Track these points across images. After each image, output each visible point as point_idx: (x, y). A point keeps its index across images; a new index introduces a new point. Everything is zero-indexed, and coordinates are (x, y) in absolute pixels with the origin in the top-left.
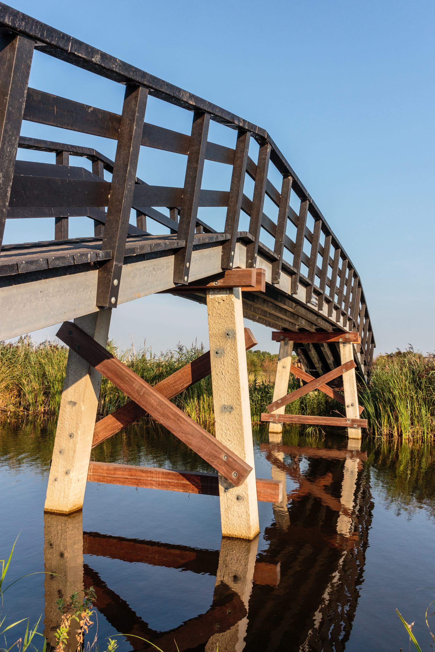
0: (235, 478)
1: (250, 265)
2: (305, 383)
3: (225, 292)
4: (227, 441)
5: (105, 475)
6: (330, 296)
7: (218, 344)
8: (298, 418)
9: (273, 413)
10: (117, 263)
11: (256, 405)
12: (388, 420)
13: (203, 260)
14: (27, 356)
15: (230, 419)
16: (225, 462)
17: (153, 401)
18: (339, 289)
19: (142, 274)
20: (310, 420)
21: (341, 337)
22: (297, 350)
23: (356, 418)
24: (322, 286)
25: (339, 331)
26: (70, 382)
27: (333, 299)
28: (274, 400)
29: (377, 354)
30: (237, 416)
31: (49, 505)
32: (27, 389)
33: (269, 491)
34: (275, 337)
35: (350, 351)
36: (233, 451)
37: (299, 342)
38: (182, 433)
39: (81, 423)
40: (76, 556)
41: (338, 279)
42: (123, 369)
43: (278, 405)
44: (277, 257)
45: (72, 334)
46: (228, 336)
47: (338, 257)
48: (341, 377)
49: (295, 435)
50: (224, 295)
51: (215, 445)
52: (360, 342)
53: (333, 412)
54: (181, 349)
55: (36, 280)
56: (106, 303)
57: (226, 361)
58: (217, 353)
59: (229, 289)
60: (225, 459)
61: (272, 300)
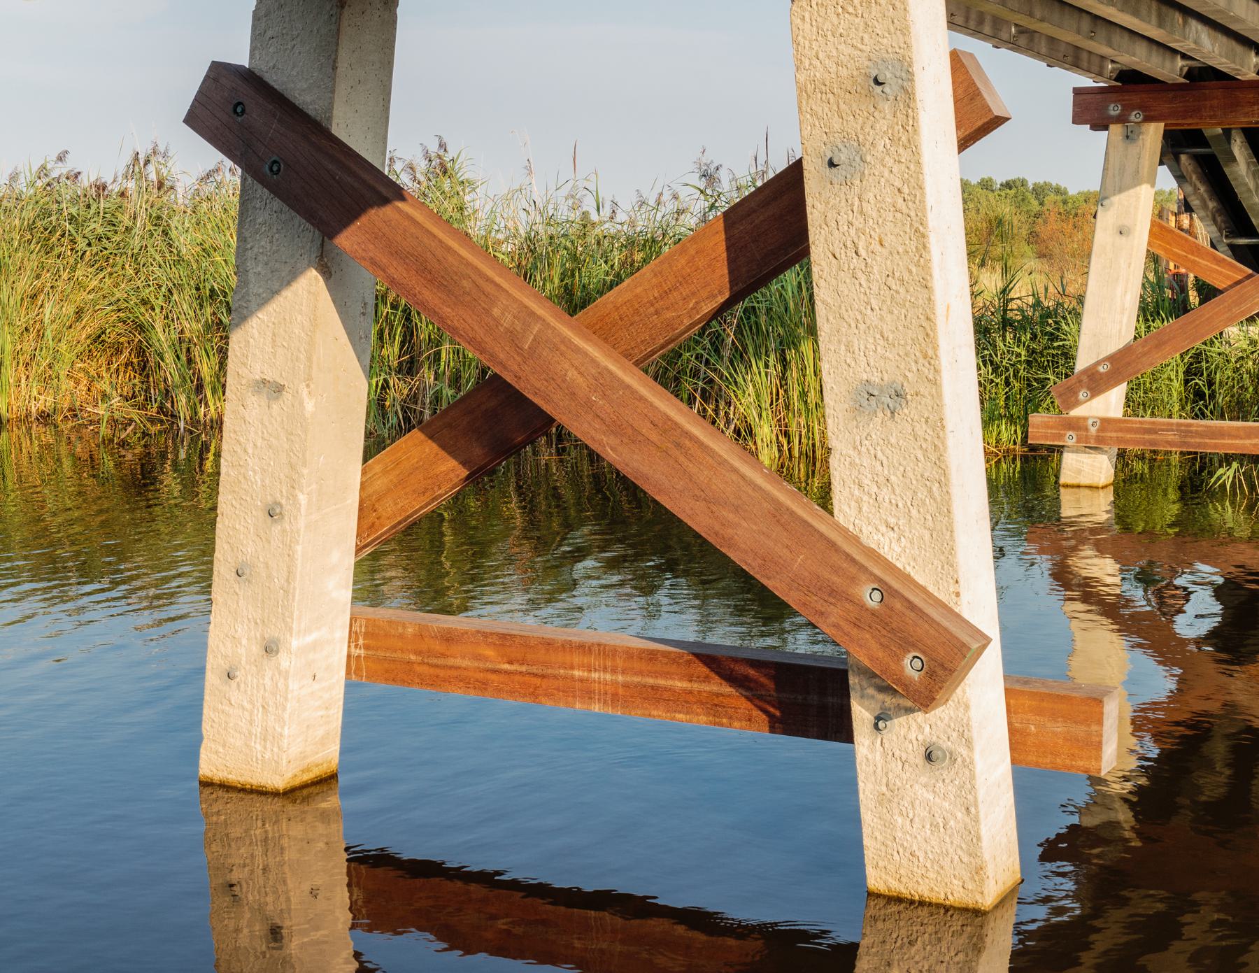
0: (916, 676)
2: (1208, 293)
4: (883, 529)
5: (413, 657)
8: (1177, 430)
11: (1007, 383)
15: (893, 441)
16: (873, 613)
17: (572, 374)
20: (1231, 436)
22: (1177, 160)
26: (253, 305)
28: (1083, 361)
30: (921, 429)
34: (1089, 110)
36: (909, 570)
37: (1189, 123)
39: (304, 464)
42: (449, 249)
43: (1096, 383)
45: (243, 111)
46: (878, 89)
51: (832, 545)
54: (709, 177)
57: (871, 196)
58: (832, 164)
60: (872, 600)
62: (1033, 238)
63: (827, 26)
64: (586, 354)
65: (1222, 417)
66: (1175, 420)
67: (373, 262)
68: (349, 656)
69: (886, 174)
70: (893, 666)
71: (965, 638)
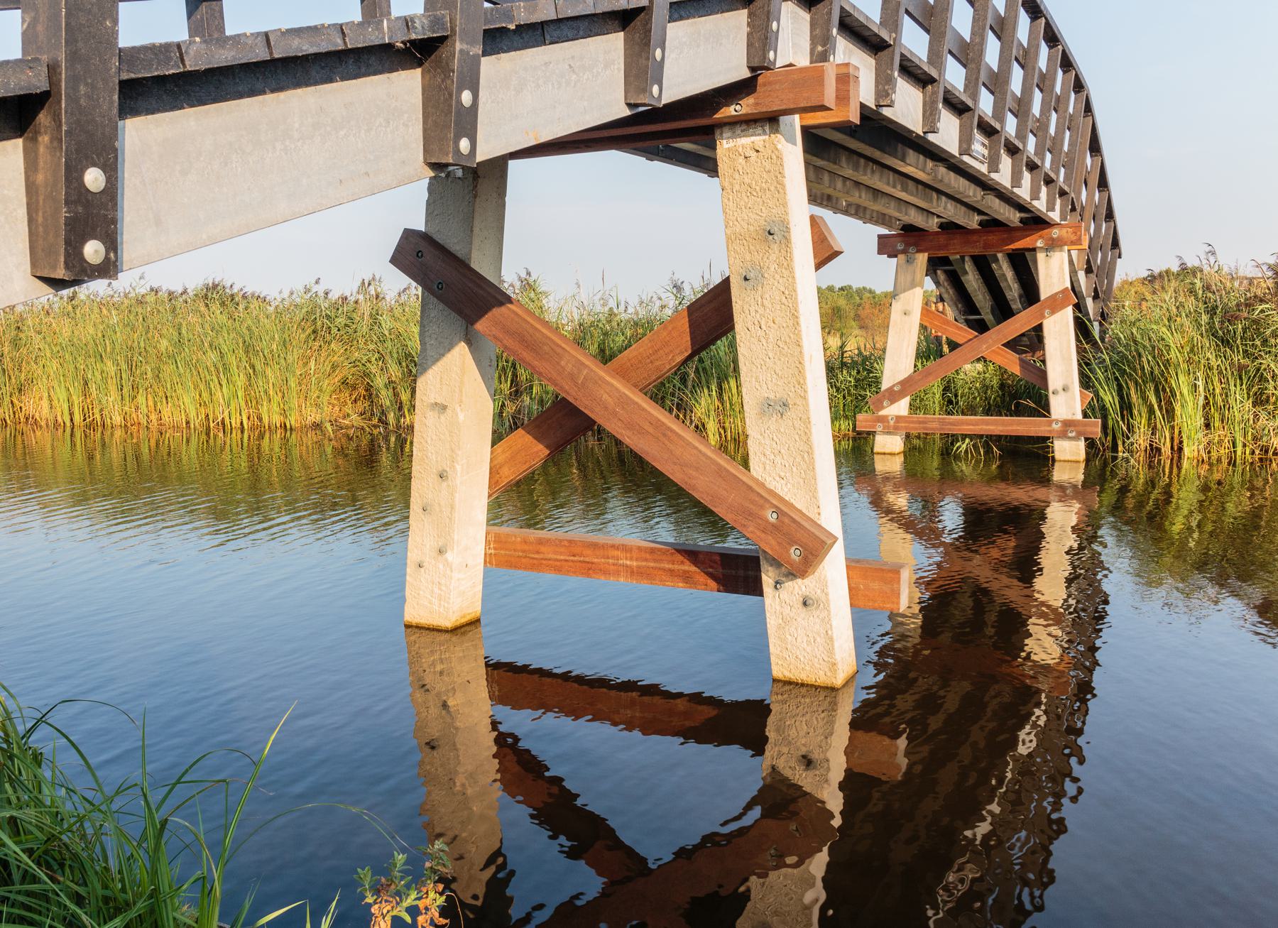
1: (821, 54)
2: (953, 346)
3: (759, 130)
6: (1017, 136)
7: (748, 258)
8: (938, 422)
9: (882, 413)
10: (465, 47)
12: (1150, 419)
13: (698, 46)
14: (375, 317)
16: (773, 525)
17: (605, 396)
18: (1038, 120)
19: (541, 82)
21: (1041, 237)
22: (936, 273)
23: (1075, 418)
24: (999, 113)
25: (1036, 222)
27: (1025, 144)
28: (885, 385)
29: (1129, 269)
31: (413, 613)
32: (379, 382)
33: (876, 585)
34: (885, 247)
35: (1062, 269)
37: (941, 254)
38: (675, 464)
40: (475, 709)
41: (1038, 96)
42: (537, 329)
43: (893, 396)
44: (887, 38)
47: (1037, 38)
48: (1039, 329)
49: (931, 460)
50: (758, 138)
51: (750, 488)
52: (1085, 245)
53: (1018, 405)
54: (678, 287)
55: (249, 96)
56: (447, 155)
58: (746, 279)
59: (770, 120)
60: (772, 518)
61: (877, 154)
62: (857, 317)
71: (824, 538)
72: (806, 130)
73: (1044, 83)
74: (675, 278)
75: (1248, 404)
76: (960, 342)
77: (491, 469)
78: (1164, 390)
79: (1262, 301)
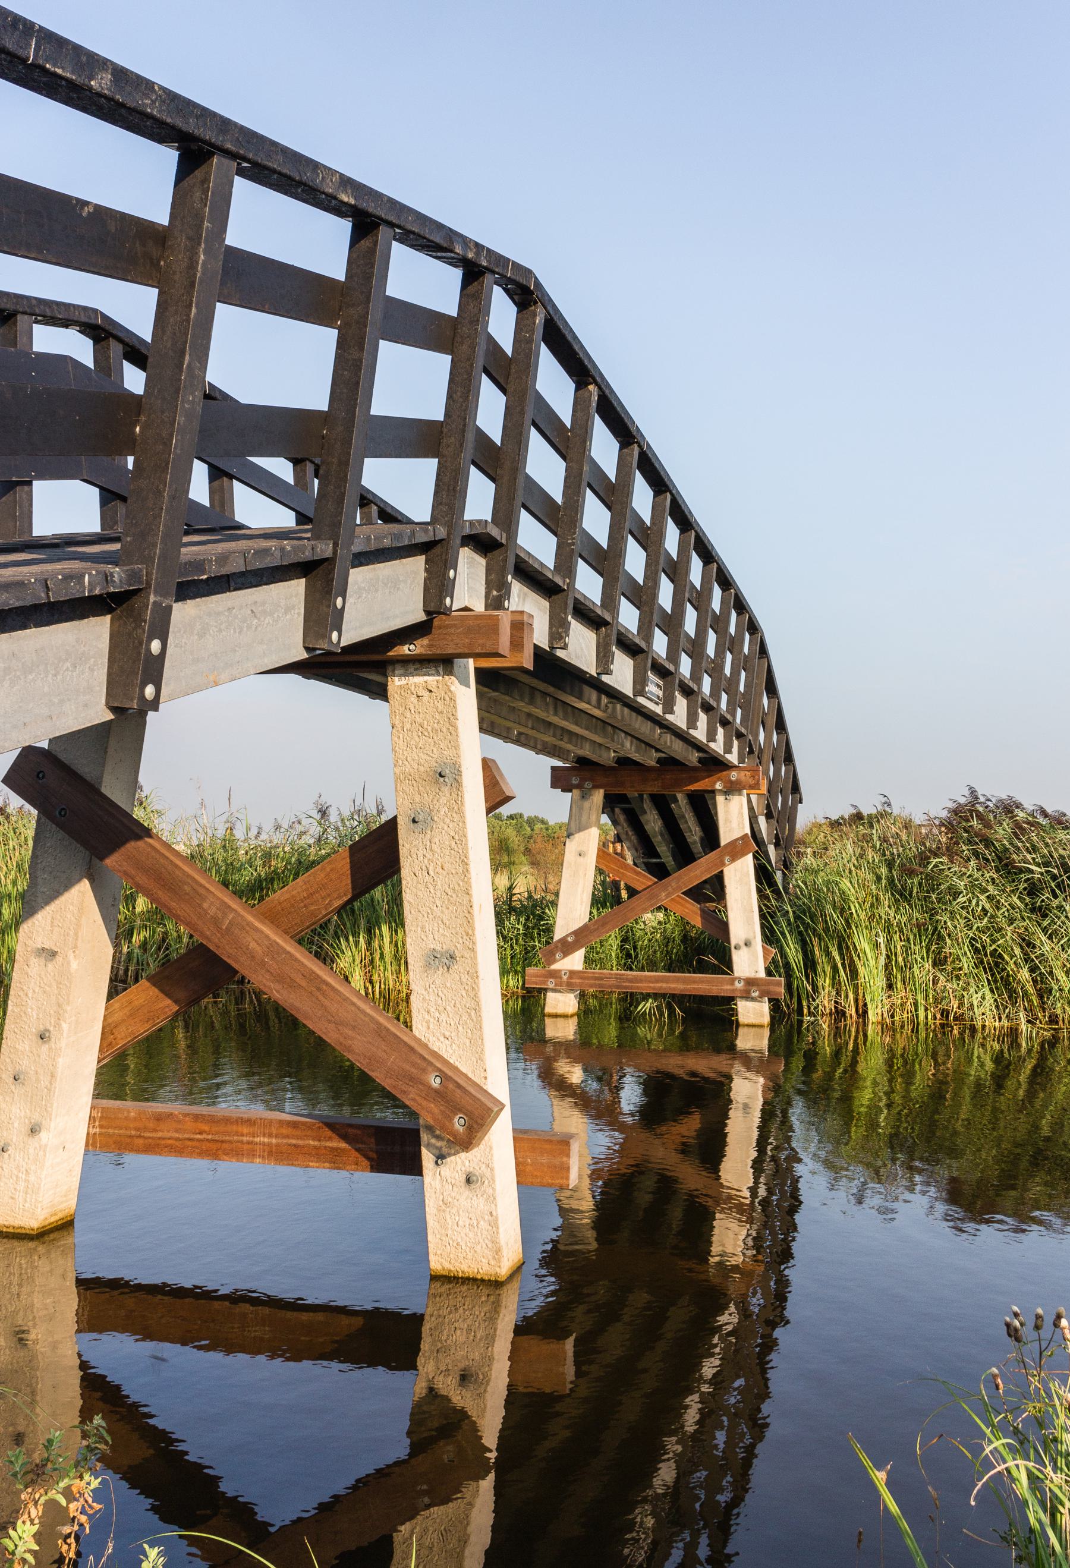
2: (632, 892)
4: (442, 1039)
9: (554, 967)
11: (512, 948)
12: (834, 978)
13: (377, 591)
15: (448, 985)
16: (436, 1091)
17: (253, 945)
18: (713, 661)
21: (719, 779)
22: (613, 811)
25: (714, 764)
27: (700, 686)
28: (558, 935)
29: (806, 816)
34: (560, 780)
35: (741, 814)
36: (457, 1064)
38: (329, 1021)
39: (68, 1003)
40: (59, 1338)
41: (712, 637)
42: (176, 866)
43: (567, 947)
44: (561, 584)
46: (442, 779)
48: (719, 878)
51: (412, 1049)
52: (764, 789)
54: (323, 813)
56: (132, 700)
57: (436, 840)
58: (414, 821)
59: (444, 663)
60: (435, 1082)
61: (551, 689)
62: (527, 851)
63: (413, 742)
64: (262, 932)
65: (642, 969)
66: (615, 971)
67: (126, 873)
68: (88, 1134)
69: (446, 827)
70: (447, 1123)
71: (490, 1105)
72: (478, 671)
73: (719, 623)
74: (322, 800)
75: (928, 966)
76: (639, 889)
77: (104, 1028)
78: (848, 947)
79: (936, 855)
